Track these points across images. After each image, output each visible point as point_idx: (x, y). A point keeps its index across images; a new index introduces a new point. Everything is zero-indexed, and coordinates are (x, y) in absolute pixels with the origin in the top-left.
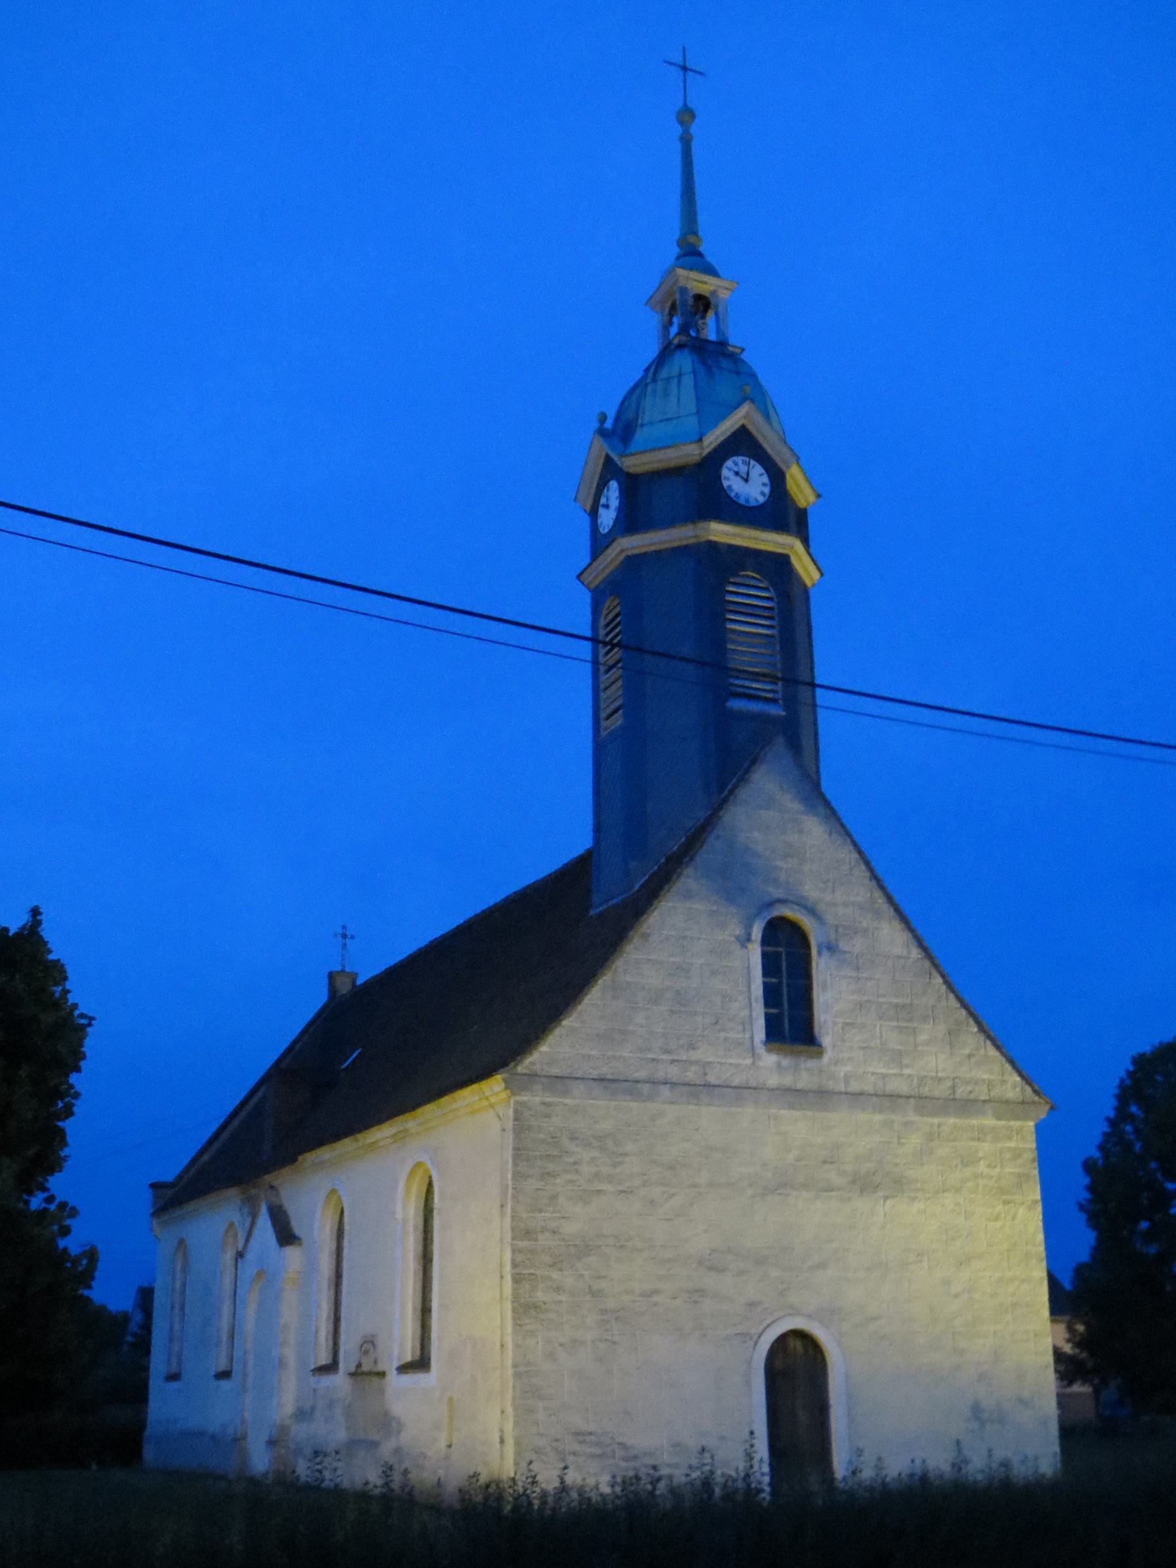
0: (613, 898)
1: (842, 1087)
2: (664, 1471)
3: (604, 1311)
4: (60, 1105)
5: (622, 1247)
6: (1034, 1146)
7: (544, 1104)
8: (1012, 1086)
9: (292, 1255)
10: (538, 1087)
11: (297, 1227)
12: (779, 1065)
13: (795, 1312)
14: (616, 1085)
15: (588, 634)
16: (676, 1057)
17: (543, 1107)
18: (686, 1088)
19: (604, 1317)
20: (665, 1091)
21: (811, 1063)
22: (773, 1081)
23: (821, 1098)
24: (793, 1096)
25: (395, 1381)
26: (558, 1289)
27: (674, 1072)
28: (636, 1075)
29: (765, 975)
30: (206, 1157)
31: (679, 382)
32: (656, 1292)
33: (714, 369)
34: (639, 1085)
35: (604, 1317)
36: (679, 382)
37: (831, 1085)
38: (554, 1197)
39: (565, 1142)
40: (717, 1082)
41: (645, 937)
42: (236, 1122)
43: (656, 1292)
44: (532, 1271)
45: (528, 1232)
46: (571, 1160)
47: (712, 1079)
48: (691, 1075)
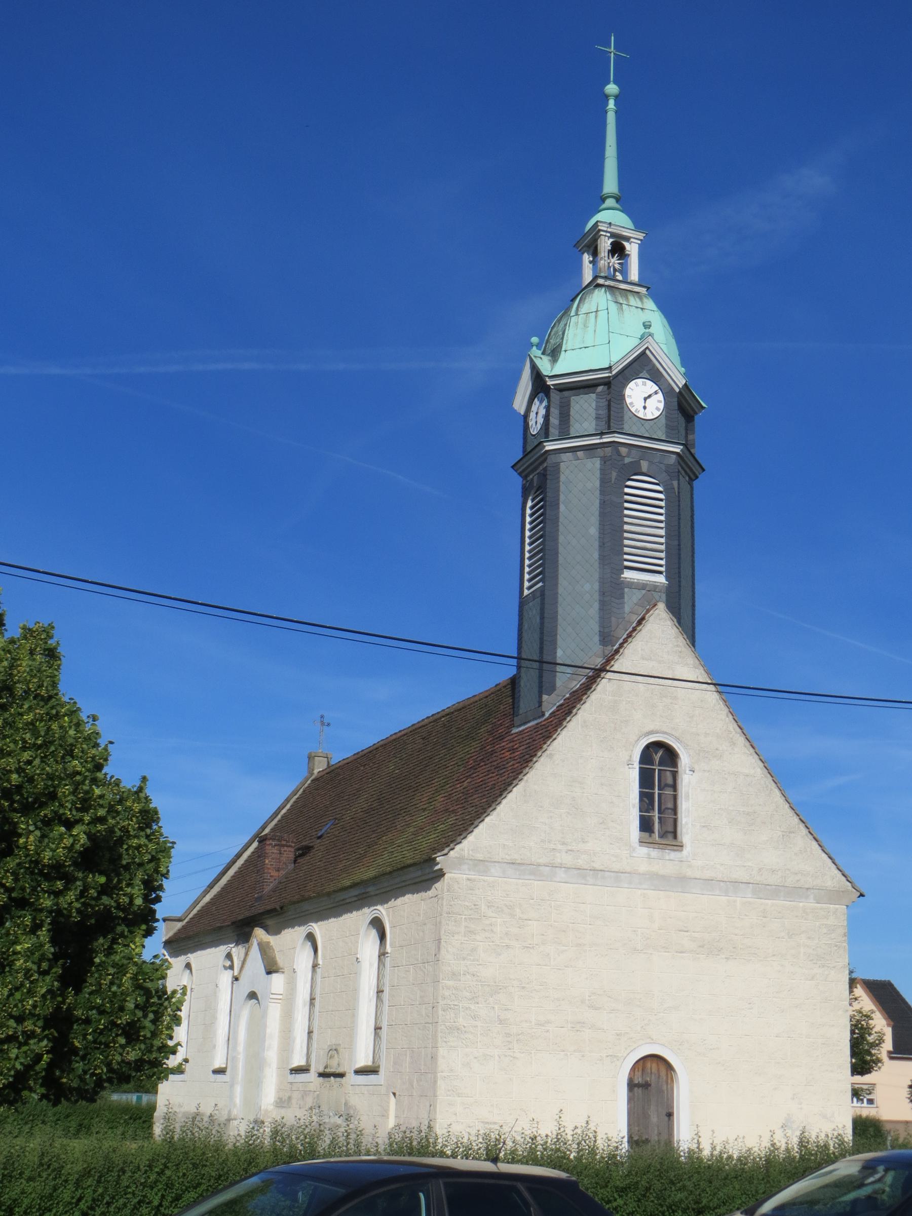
0: (529, 722)
1: (698, 874)
2: (130, 1158)
3: (508, 1035)
4: (154, 896)
5: (523, 988)
6: (845, 924)
7: (468, 879)
8: (832, 878)
9: (277, 981)
10: (465, 867)
11: (280, 960)
12: (649, 855)
13: (653, 1042)
14: (523, 867)
15: (516, 655)
16: (570, 848)
17: (468, 882)
18: (575, 872)
19: (509, 1039)
20: (561, 874)
21: (673, 855)
22: (643, 868)
23: (681, 882)
24: (660, 881)
25: (351, 1078)
26: (475, 1017)
27: (567, 859)
28: (541, 861)
29: (640, 787)
30: (208, 898)
31: (596, 317)
32: (548, 1022)
33: (624, 307)
34: (541, 868)
35: (509, 1039)
36: (596, 317)
37: (689, 873)
38: (474, 950)
39: (483, 907)
40: (601, 868)
41: (551, 756)
42: (231, 872)
43: (548, 1022)
44: (456, 1003)
45: (454, 974)
46: (488, 922)
47: (597, 866)
48: (580, 862)
